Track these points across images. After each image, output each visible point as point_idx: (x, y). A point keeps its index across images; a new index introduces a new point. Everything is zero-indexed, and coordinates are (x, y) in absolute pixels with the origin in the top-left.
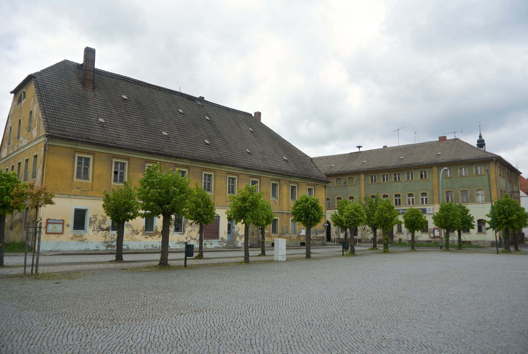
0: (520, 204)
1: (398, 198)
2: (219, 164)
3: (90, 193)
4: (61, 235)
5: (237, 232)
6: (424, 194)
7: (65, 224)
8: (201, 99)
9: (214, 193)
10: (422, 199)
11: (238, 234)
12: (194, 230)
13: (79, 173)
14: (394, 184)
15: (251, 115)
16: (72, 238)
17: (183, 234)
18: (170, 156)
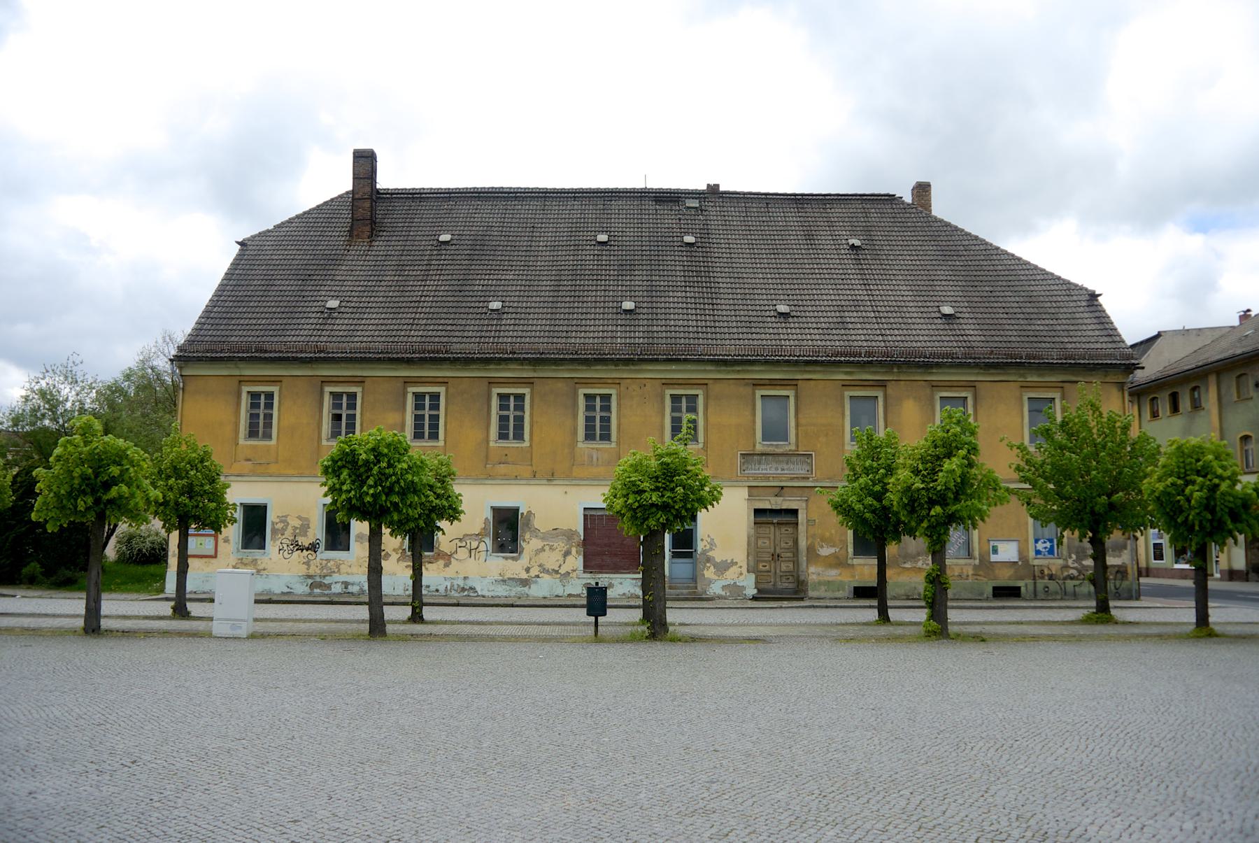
0: (347, 193)
3: (273, 468)
4: (213, 561)
5: (704, 552)
8: (713, 190)
9: (618, 443)
11: (709, 560)
12: (551, 548)
15: (891, 199)
18: (467, 361)
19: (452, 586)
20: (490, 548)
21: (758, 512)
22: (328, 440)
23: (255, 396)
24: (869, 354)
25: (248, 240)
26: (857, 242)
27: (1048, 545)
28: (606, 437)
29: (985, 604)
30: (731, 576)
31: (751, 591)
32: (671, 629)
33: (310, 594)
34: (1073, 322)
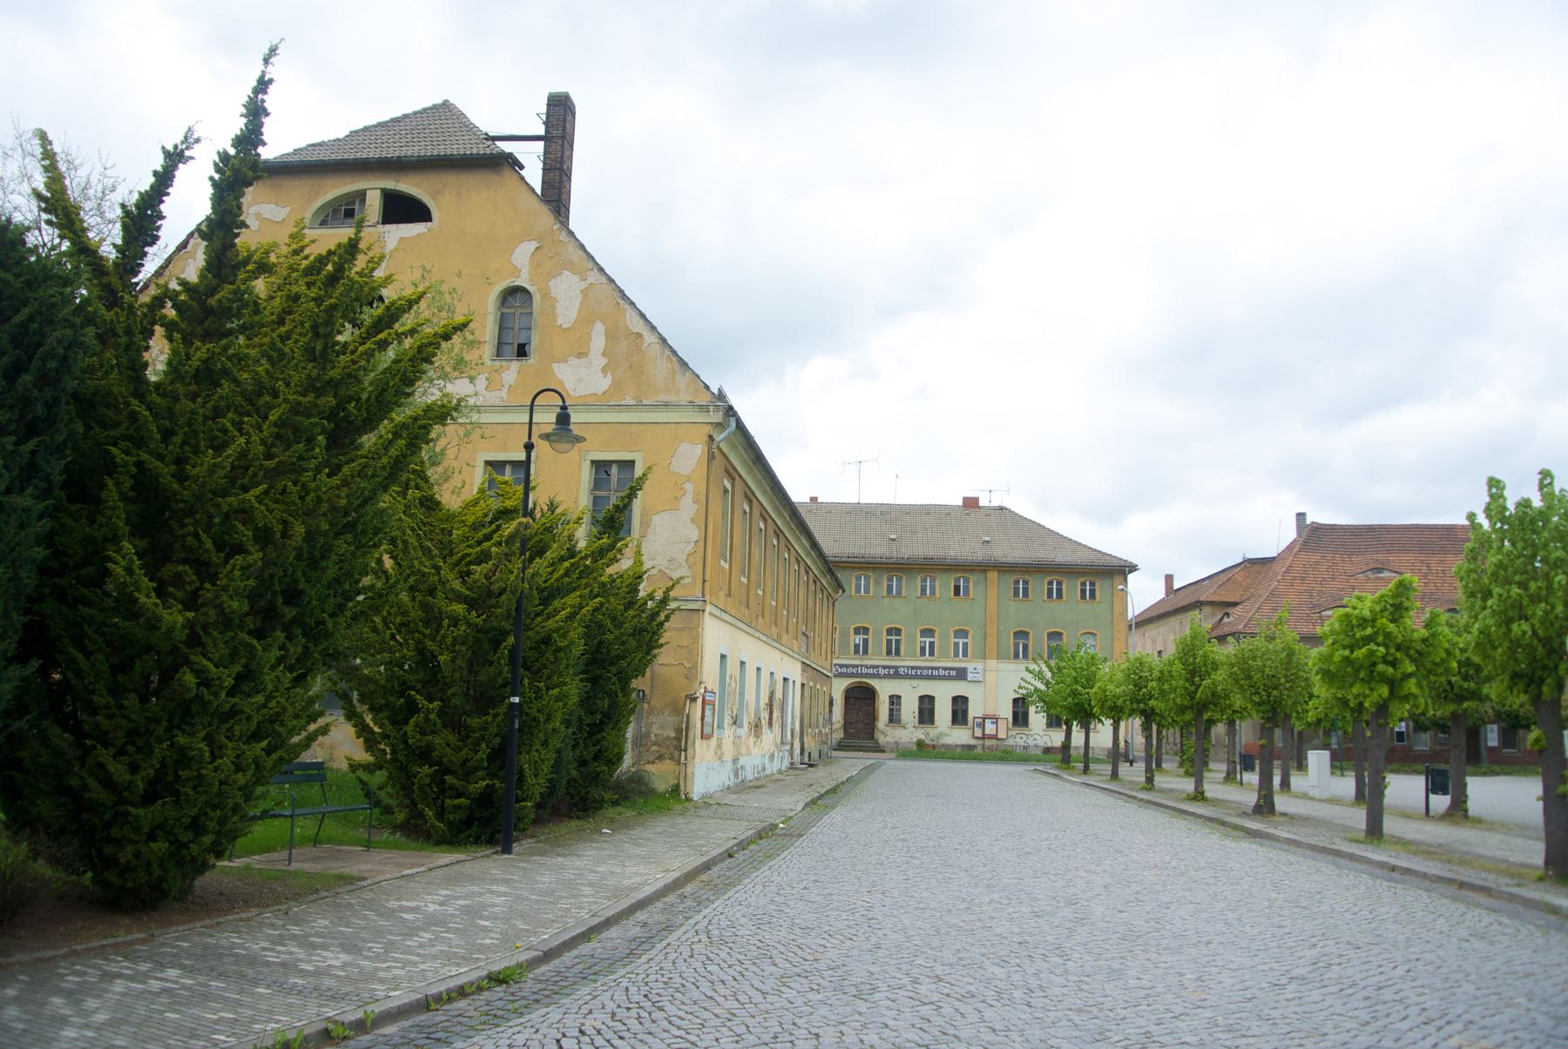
1: (893, 638)
6: (962, 633)
10: (956, 644)
14: (886, 601)
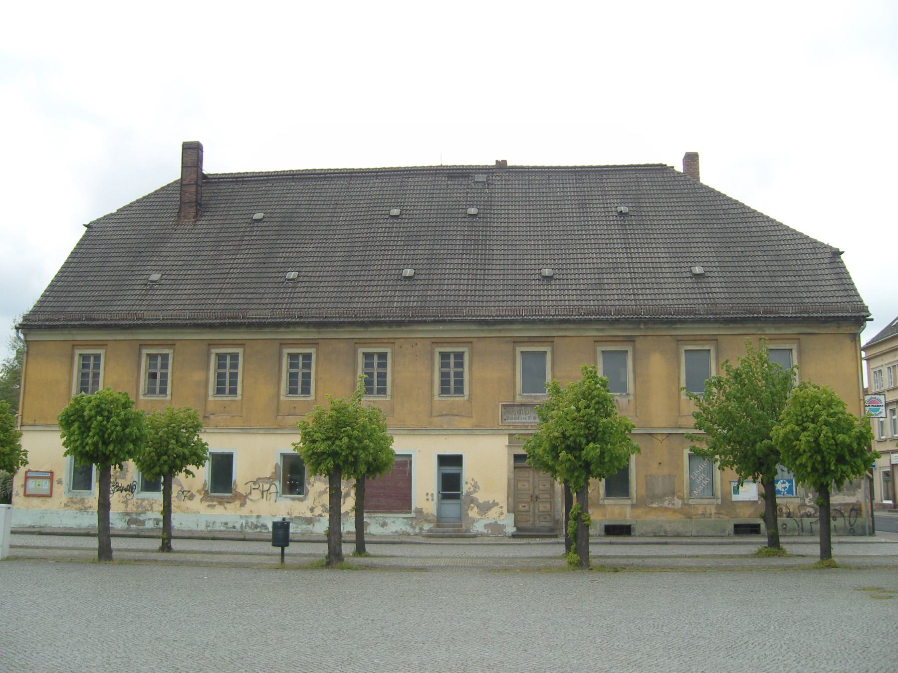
0: (176, 182)
2: (400, 323)
4: (48, 499)
5: (468, 494)
7: (56, 478)
8: (501, 166)
9: (392, 396)
11: (473, 501)
13: (445, 383)
16: (66, 505)
17: (301, 500)
18: (260, 325)
19: (247, 523)
20: (280, 490)
21: (518, 458)
22: (145, 395)
23: (85, 357)
24: (618, 312)
25: (94, 222)
26: (624, 209)
27: (787, 485)
28: (382, 391)
29: (725, 540)
30: (493, 515)
31: (511, 529)
32: (346, 559)
33: (128, 529)
34: (814, 278)
